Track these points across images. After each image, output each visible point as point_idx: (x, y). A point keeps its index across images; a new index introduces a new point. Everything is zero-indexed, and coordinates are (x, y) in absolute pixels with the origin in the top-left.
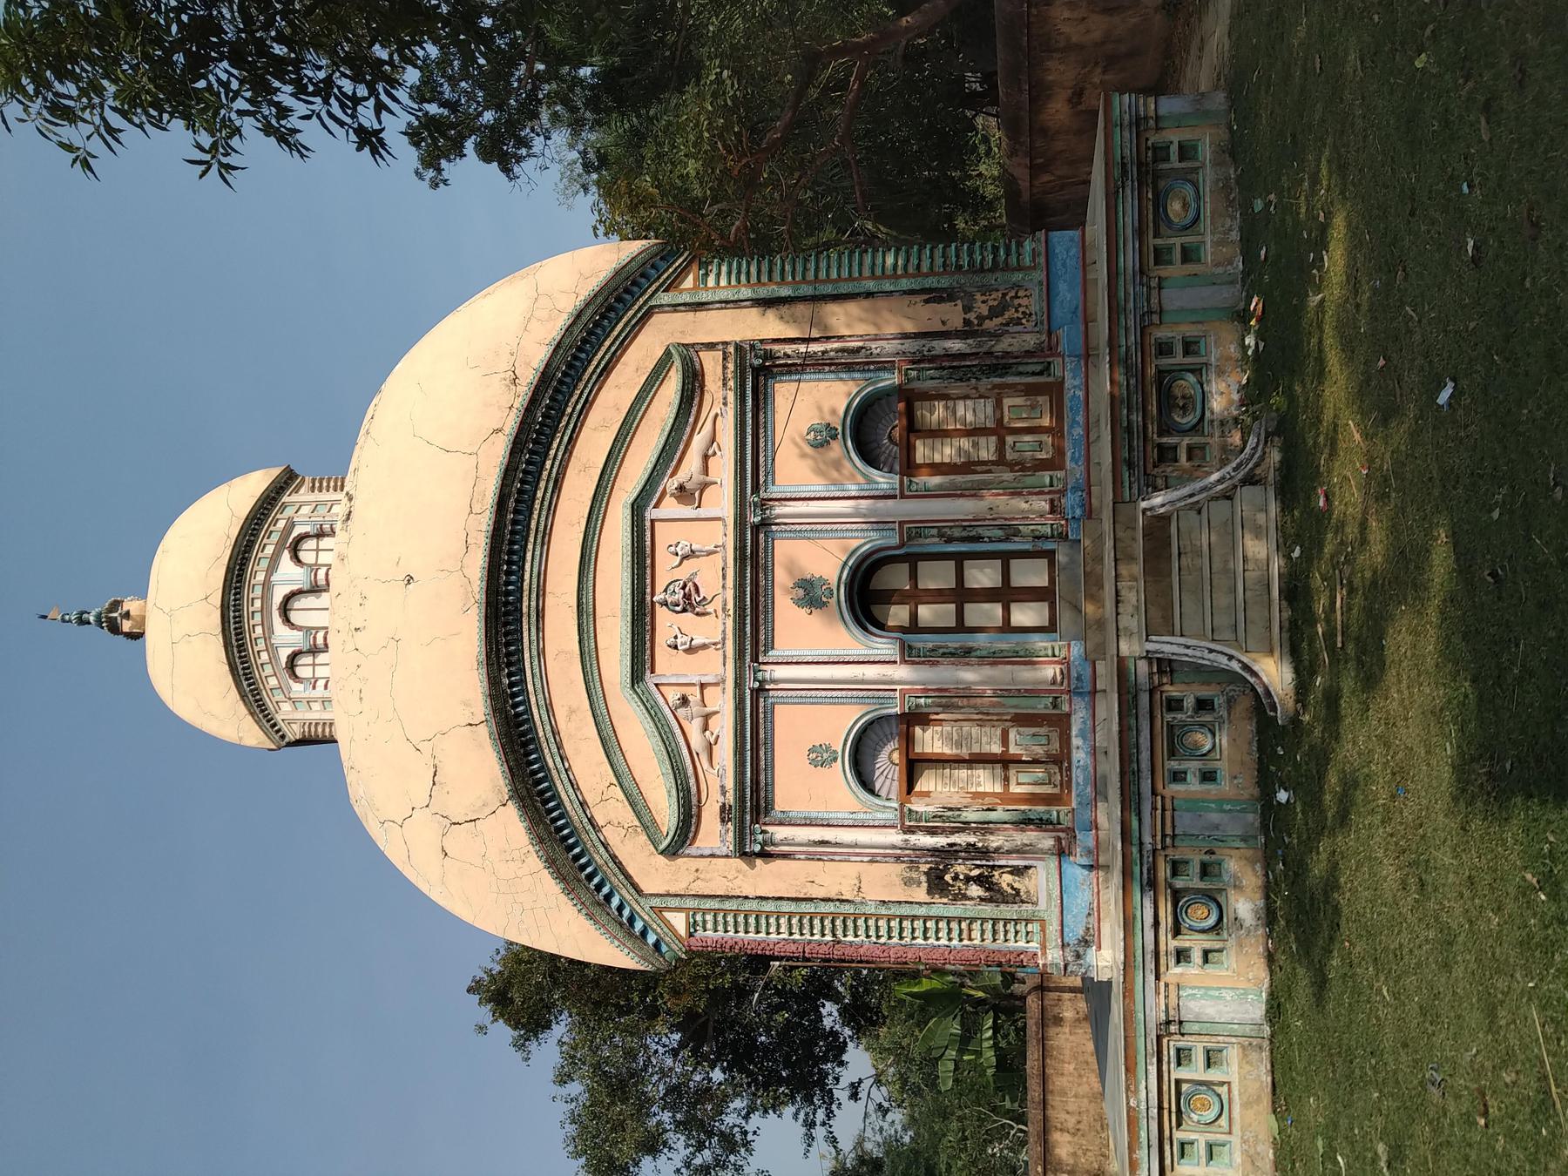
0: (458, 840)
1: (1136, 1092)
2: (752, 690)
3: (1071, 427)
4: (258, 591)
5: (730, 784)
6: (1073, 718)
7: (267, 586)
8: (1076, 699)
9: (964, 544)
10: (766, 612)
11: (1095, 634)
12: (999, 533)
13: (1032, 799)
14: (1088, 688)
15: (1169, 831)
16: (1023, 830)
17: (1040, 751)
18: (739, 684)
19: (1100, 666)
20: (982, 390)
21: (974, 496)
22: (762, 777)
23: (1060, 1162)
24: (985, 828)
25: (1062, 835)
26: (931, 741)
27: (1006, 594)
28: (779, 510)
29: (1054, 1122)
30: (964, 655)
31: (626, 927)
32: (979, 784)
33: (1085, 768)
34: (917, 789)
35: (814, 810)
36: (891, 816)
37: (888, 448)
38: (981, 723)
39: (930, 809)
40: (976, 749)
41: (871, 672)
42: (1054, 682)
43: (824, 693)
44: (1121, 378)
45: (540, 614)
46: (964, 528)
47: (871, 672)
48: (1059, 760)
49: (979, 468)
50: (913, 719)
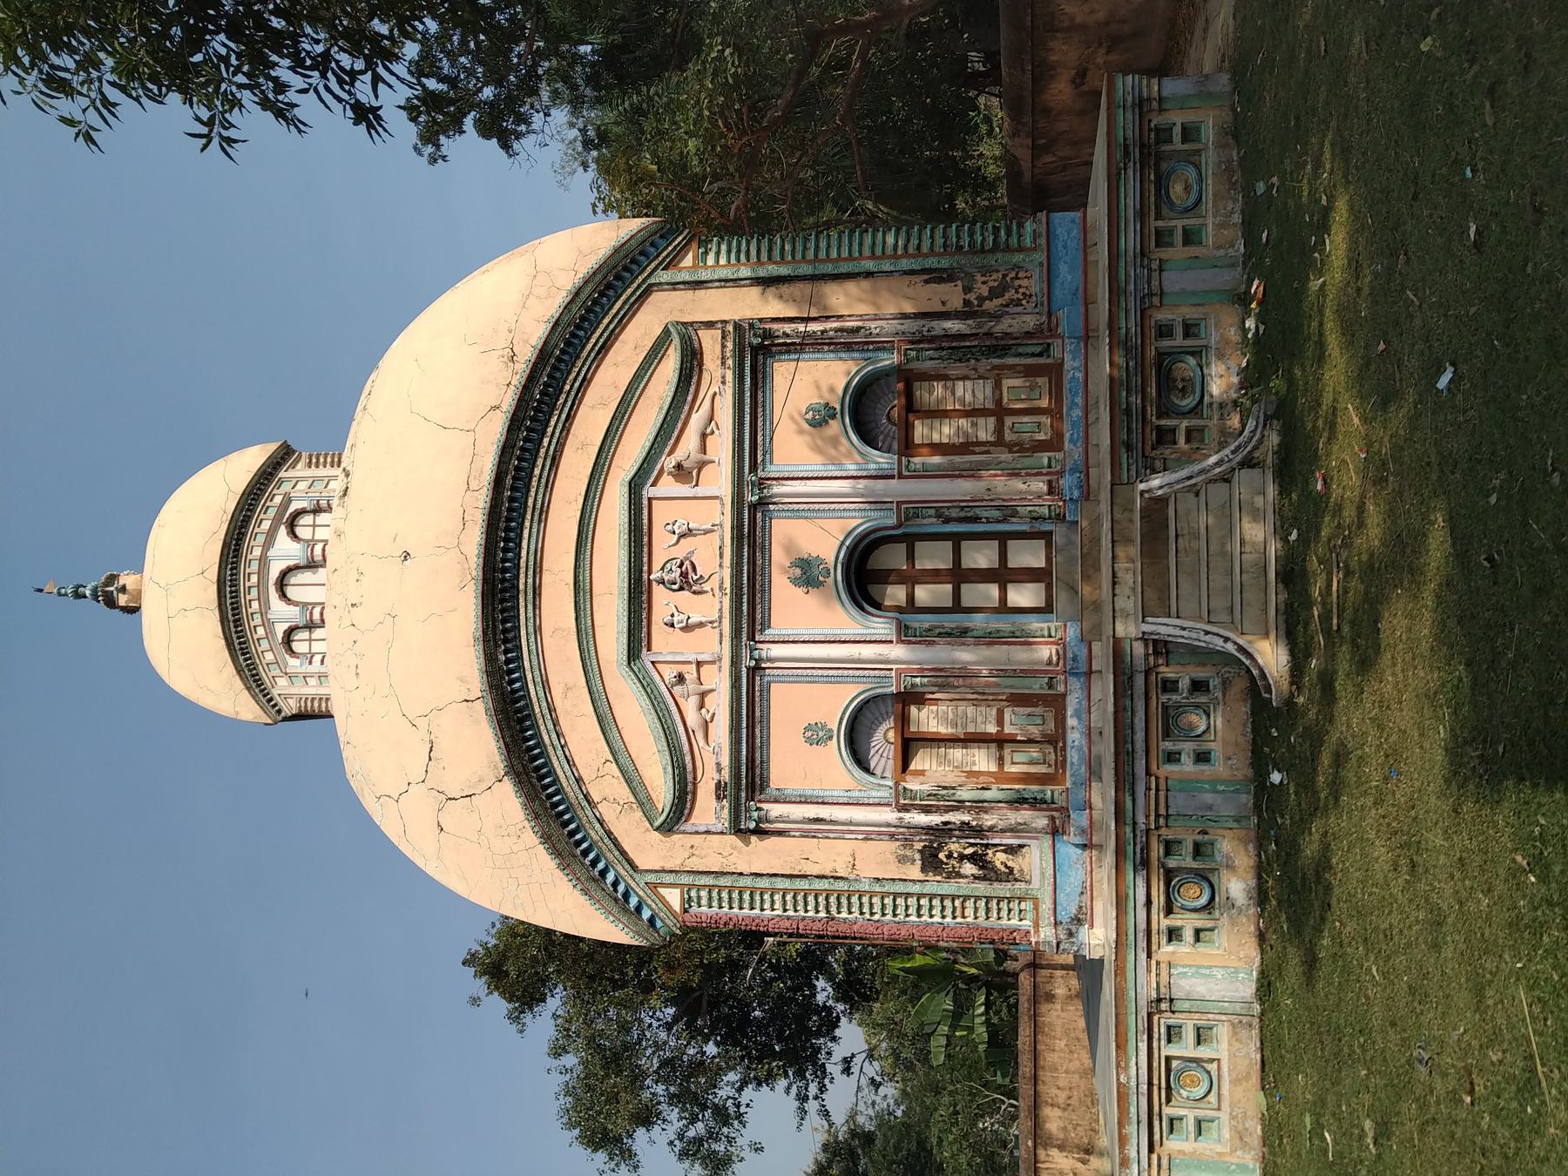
0: (454, 815)
1: (1127, 1068)
2: (748, 669)
3: (1070, 409)
4: (255, 566)
5: (725, 761)
6: (1068, 698)
7: (264, 561)
8: (1071, 680)
9: (960, 525)
10: (763, 591)
12: (997, 514)
13: (1027, 778)
14: (1083, 668)
15: (1162, 811)
16: (1017, 809)
18: (735, 662)
19: (1096, 647)
20: (981, 371)
22: (758, 755)
23: (1050, 1137)
25: (1056, 814)
26: (928, 719)
27: (1003, 575)
29: (1044, 1097)
30: (960, 635)
31: (621, 903)
33: (1080, 749)
34: (912, 767)
35: (810, 788)
36: (885, 794)
39: (925, 787)
40: (971, 729)
43: (820, 672)
44: (1121, 361)
45: (537, 591)
48: (1055, 740)
49: (977, 449)
50: (909, 698)
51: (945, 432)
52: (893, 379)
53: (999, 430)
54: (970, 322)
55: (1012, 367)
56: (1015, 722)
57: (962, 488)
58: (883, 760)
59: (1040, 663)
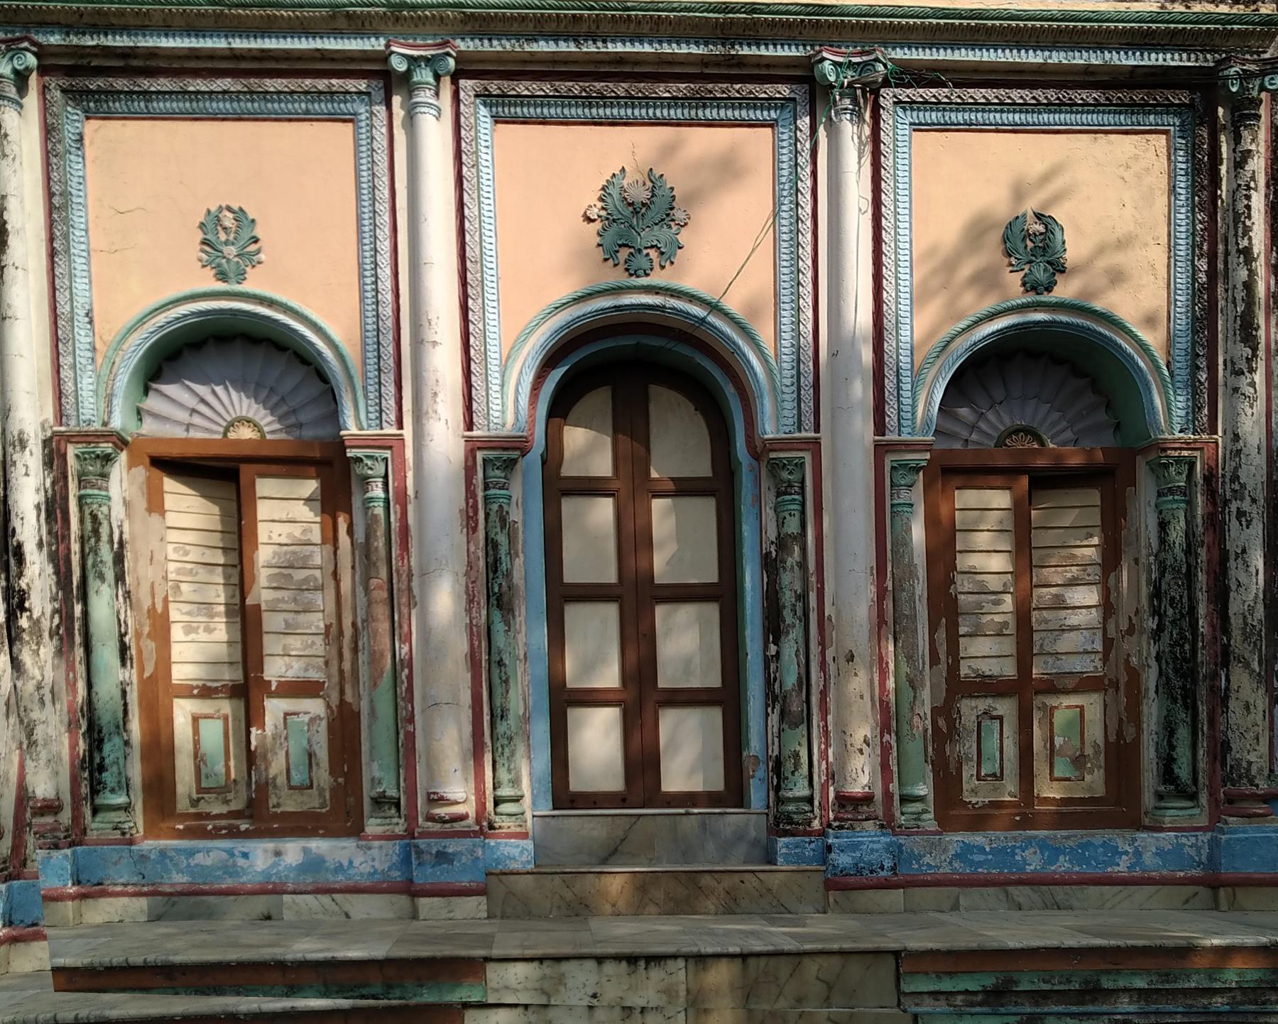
2: (384, 57)
3: (1043, 845)
6: (349, 844)
8: (395, 848)
9: (763, 601)
10: (587, 100)
11: (557, 891)
12: (790, 679)
13: (159, 749)
14: (424, 875)
16: (72, 726)
17: (276, 766)
19: (473, 907)
20: (1128, 645)
21: (881, 621)
22: (164, 84)
24: (74, 632)
25: (66, 817)
26: (285, 514)
27: (642, 698)
28: (851, 134)
30: (492, 593)
32: (189, 629)
33: (231, 870)
34: (169, 484)
36: (89, 411)
37: (987, 425)
38: (332, 634)
39: (118, 512)
40: (271, 622)
41: (443, 362)
42: (436, 800)
43: (385, 246)
44: (1230, 977)
46: (803, 597)
47: (443, 362)
48: (258, 815)
49: (941, 635)
50: (333, 472)
51: (987, 558)
52: (1109, 440)
53: (989, 687)
54: (1260, 612)
55: (1134, 713)
56: (292, 725)
57: (852, 594)
58: (183, 416)
59: (432, 775)
